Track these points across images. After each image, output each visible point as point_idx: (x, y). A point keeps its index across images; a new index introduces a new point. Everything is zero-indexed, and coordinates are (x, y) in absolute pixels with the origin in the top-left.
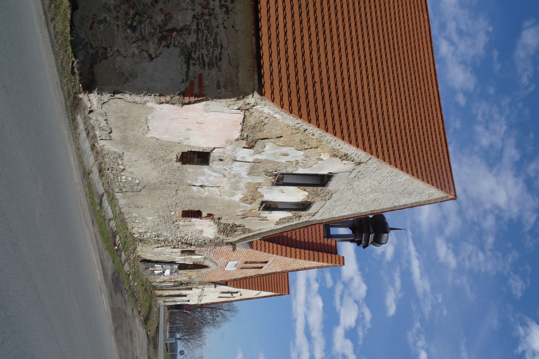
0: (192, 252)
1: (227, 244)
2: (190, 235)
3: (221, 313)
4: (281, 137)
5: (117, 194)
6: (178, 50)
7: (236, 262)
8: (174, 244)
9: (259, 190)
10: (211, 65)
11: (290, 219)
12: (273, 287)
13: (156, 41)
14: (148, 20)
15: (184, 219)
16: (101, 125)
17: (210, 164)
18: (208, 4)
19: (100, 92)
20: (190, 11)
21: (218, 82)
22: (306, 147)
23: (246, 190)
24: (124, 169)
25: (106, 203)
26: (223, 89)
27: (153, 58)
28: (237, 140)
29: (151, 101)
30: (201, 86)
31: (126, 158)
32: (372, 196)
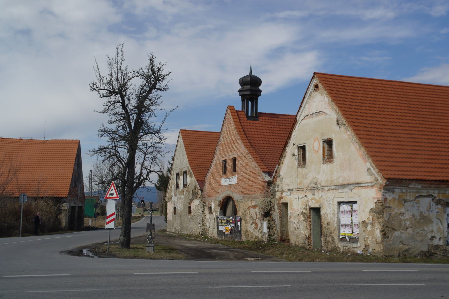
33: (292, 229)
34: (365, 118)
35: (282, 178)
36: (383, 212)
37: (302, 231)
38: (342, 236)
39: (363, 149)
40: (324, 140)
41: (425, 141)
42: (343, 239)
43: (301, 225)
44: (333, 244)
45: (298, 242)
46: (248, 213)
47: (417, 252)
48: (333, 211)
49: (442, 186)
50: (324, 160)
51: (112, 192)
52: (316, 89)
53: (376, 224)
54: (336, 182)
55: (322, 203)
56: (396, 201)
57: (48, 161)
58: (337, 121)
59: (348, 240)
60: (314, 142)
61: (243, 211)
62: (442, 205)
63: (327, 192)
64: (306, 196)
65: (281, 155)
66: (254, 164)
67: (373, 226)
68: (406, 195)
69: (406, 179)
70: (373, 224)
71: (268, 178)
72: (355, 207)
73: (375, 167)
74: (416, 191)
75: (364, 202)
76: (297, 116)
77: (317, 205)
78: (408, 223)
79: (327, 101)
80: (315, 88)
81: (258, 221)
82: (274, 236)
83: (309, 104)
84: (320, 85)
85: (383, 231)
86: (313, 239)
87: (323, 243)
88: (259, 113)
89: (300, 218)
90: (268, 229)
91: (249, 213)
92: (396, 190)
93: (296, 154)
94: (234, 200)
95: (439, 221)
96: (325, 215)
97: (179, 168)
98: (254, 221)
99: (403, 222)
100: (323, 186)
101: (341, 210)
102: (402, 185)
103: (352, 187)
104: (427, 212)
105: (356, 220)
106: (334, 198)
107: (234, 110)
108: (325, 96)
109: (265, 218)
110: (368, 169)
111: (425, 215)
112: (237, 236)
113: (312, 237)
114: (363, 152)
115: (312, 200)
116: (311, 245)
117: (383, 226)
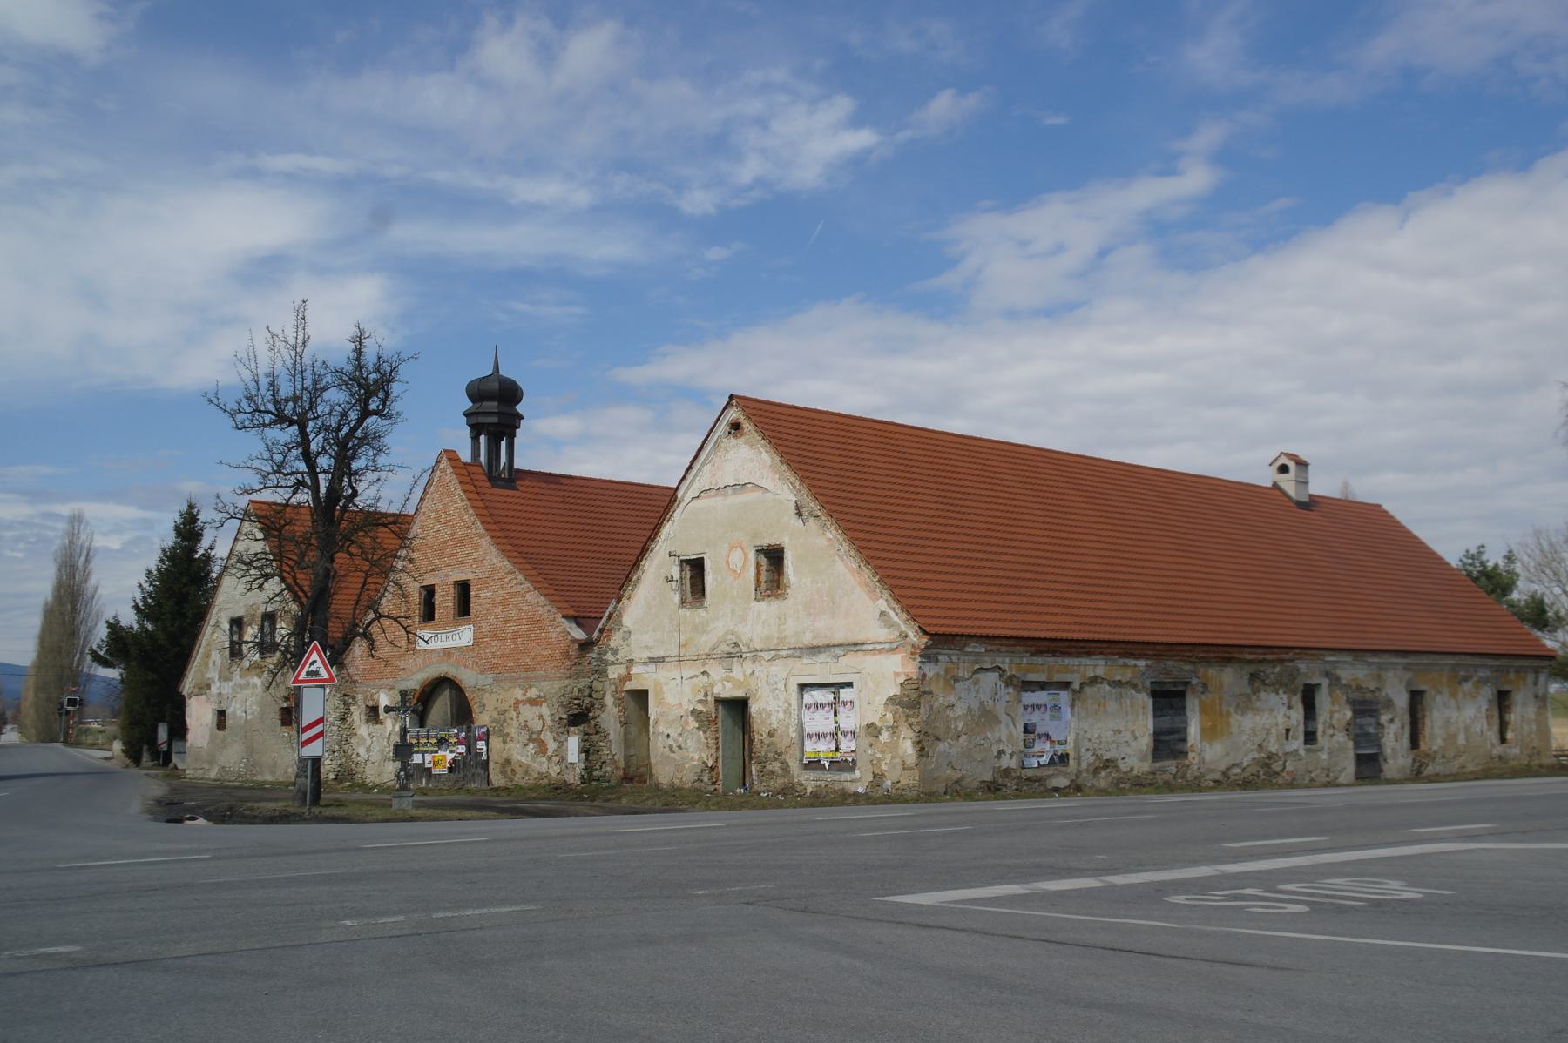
33: (661, 750)
35: (630, 632)
36: (919, 703)
37: (692, 752)
38: (810, 758)
39: (867, 572)
40: (760, 548)
41: (993, 557)
42: (814, 765)
43: (688, 741)
44: (784, 776)
45: (678, 779)
46: (512, 719)
47: (975, 784)
48: (786, 705)
49: (1018, 647)
50: (758, 593)
51: (314, 668)
52: (733, 431)
53: (901, 729)
54: (793, 640)
55: (754, 688)
56: (942, 681)
58: (797, 508)
59: (827, 768)
60: (730, 551)
61: (495, 714)
62: (1015, 687)
63: (770, 663)
64: (703, 673)
65: (628, 579)
66: (535, 597)
67: (894, 732)
68: (958, 668)
69: (962, 635)
70: (895, 730)
71: (579, 634)
72: (845, 694)
73: (899, 611)
74: (974, 658)
75: (871, 684)
76: (678, 488)
77: (739, 694)
78: (960, 725)
79: (769, 462)
80: (731, 428)
81: (548, 737)
82: (603, 770)
83: (713, 465)
84: (746, 425)
85: (919, 742)
86: (723, 770)
87: (754, 778)
88: (519, 471)
89: (687, 724)
90: (583, 755)
91: (518, 717)
92: (940, 657)
93: (677, 576)
94: (462, 686)
95: (1010, 719)
96: (761, 714)
97: (241, 604)
98: (534, 736)
99: (953, 722)
100: (757, 651)
101: (805, 702)
102: (953, 647)
103: (839, 651)
104: (991, 702)
105: (848, 721)
106: (787, 675)
107: (459, 460)
108: (761, 449)
109: (572, 729)
110: (882, 614)
111: (988, 709)
112: (473, 775)
113: (720, 765)
114: (869, 577)
115: (726, 683)
116: (718, 783)
117: (919, 732)
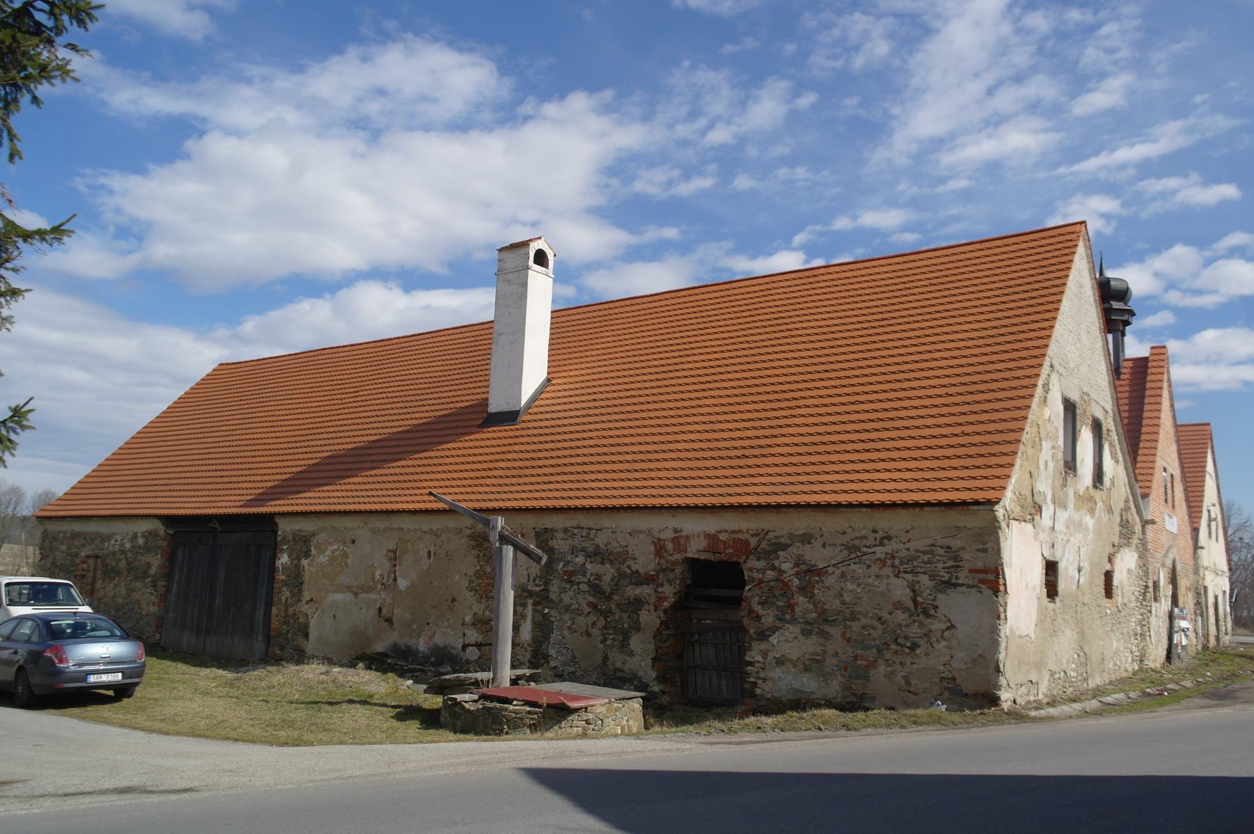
0: (1156, 585)
1: (1144, 532)
2: (1134, 588)
3: (1234, 533)
4: (1030, 473)
5: (1090, 686)
6: (940, 596)
7: (1167, 517)
8: (1145, 611)
9: (1081, 494)
10: (956, 558)
11: (1111, 445)
12: (1197, 451)
13: (929, 620)
14: (904, 629)
15: (1114, 596)
16: (1026, 692)
17: (1057, 560)
18: (880, 560)
19: (999, 687)
20: (889, 581)
21: (978, 550)
22: (1038, 439)
23: (1083, 511)
24: (1065, 672)
25: (1109, 699)
26: (988, 545)
27: (952, 624)
28: (1034, 526)
29: (1005, 630)
30: (985, 571)
31: (1054, 668)
32: (1084, 338)
34: (352, 358)
57: (249, 448)
